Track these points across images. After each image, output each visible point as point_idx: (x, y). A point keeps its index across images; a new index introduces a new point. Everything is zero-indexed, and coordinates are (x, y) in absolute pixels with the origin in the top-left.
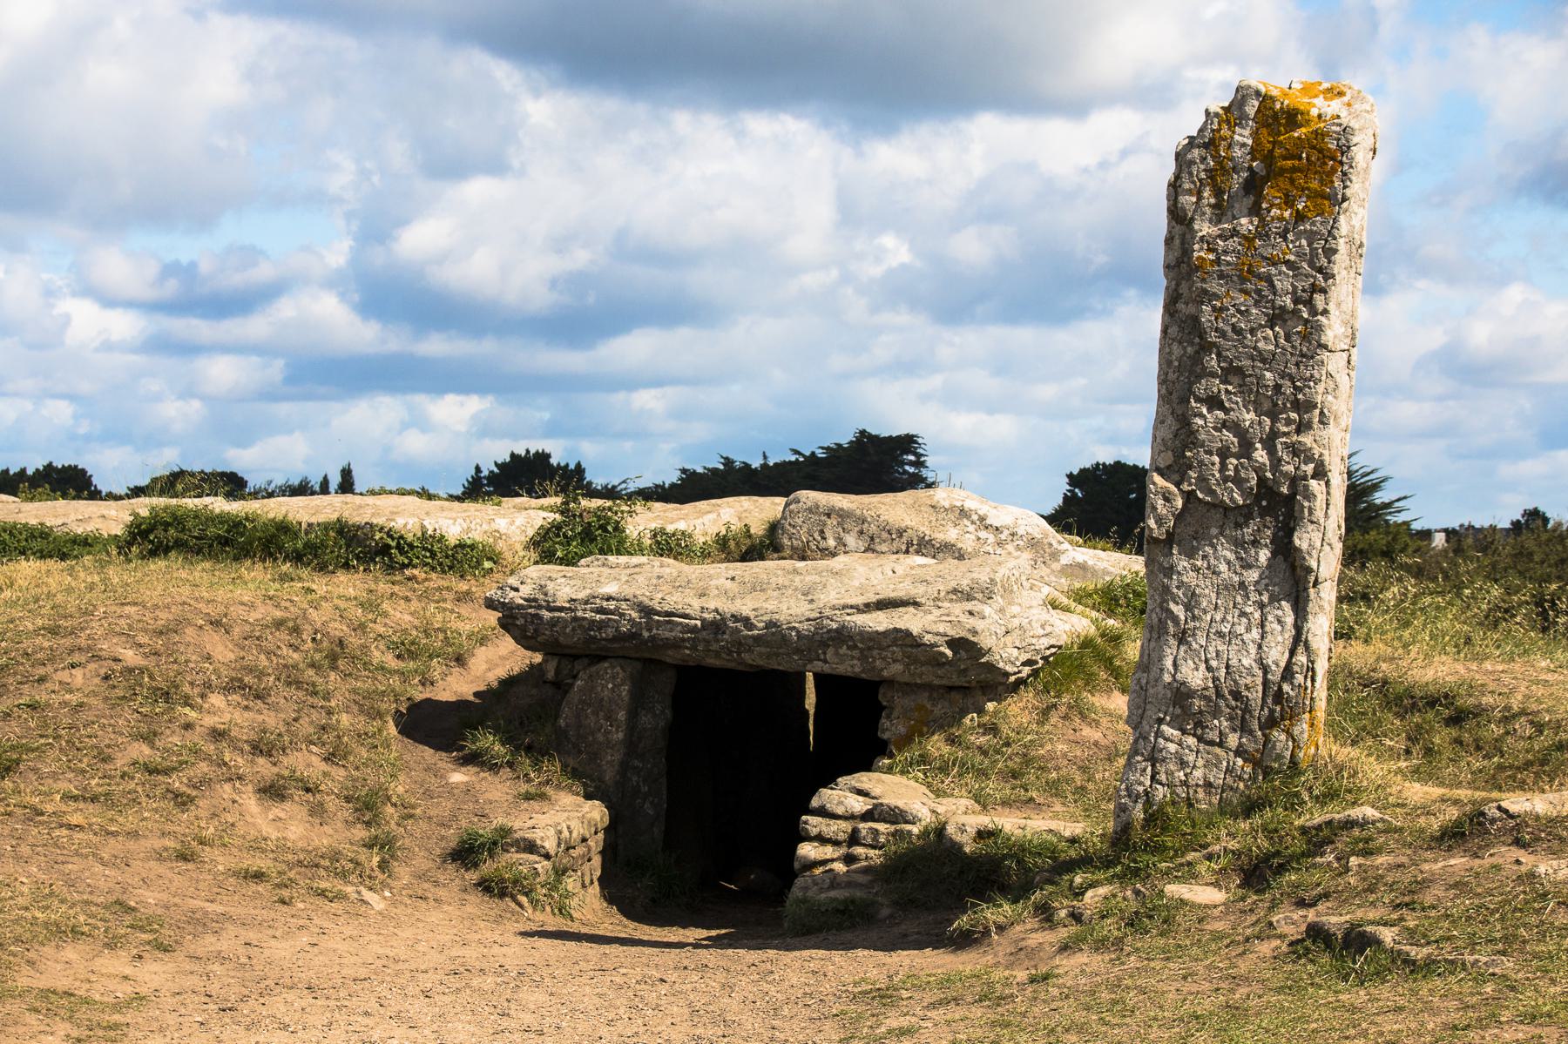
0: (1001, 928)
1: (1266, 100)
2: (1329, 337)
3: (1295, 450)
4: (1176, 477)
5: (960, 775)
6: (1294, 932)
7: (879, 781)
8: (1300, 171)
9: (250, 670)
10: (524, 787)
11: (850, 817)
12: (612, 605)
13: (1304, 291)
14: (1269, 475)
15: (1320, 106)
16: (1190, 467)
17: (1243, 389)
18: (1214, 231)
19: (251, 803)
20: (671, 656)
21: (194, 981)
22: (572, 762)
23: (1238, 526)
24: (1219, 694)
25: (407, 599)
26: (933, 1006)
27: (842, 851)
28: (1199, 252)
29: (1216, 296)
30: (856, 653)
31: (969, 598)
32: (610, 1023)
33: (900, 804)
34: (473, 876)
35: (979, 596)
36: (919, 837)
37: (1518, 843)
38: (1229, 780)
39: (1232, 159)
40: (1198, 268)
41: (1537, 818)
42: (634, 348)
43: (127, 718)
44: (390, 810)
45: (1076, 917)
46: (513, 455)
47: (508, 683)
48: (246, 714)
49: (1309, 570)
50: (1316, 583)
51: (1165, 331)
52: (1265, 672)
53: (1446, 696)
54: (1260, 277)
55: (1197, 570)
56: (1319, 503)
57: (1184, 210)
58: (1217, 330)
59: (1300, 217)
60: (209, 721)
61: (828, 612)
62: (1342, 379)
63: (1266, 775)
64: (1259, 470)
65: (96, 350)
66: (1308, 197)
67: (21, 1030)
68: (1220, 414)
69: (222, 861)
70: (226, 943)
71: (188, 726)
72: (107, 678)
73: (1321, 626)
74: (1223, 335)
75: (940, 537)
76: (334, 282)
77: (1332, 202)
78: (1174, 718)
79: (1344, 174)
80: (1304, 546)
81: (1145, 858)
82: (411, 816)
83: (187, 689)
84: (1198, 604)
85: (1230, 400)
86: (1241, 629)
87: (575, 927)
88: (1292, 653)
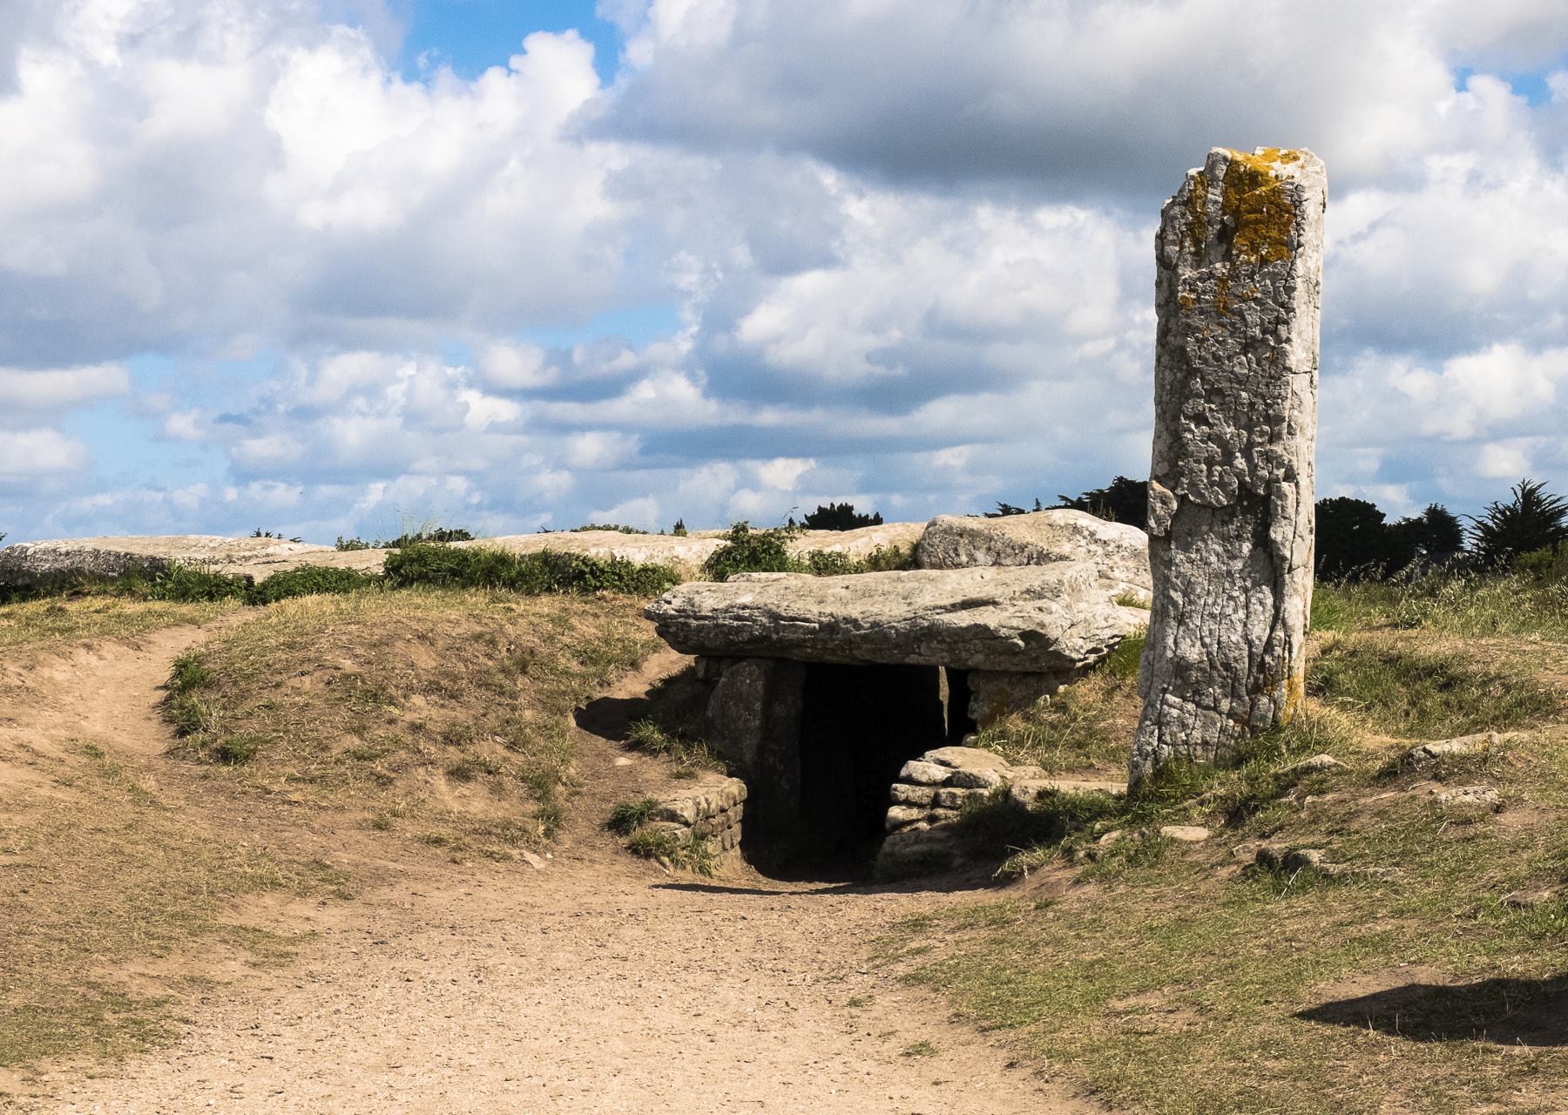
0: (1032, 869)
1: (1232, 164)
2: (1292, 361)
3: (1269, 458)
4: (1172, 484)
5: (1033, 747)
6: (1248, 858)
7: (962, 753)
9: (446, 675)
10: (675, 768)
11: (932, 784)
12: (747, 613)
15: (1278, 169)
16: (1183, 475)
17: (1223, 407)
19: (441, 783)
20: (796, 655)
21: (363, 923)
22: (717, 746)
23: (1224, 523)
24: (1213, 667)
25: (596, 616)
26: (953, 931)
27: (926, 812)
28: (1183, 293)
29: (1198, 330)
30: (944, 646)
31: (1040, 596)
32: (686, 950)
33: (975, 771)
34: (624, 841)
35: (1049, 595)
36: (989, 799)
37: (1437, 778)
38: (1223, 739)
39: (1206, 214)
41: (1453, 756)
42: (941, 413)
43: (343, 715)
44: (560, 788)
45: (1091, 856)
46: (820, 509)
47: (669, 682)
48: (443, 711)
49: (1284, 559)
50: (1290, 570)
51: (1158, 360)
52: (1250, 647)
53: (1442, 666)
54: (1233, 312)
55: (1192, 562)
56: (1291, 498)
59: (1264, 261)
60: (409, 717)
61: (921, 612)
62: (1306, 396)
63: (1252, 733)
64: (1240, 475)
65: (486, 432)
67: (211, 956)
69: (410, 829)
70: (399, 893)
71: (391, 721)
72: (329, 683)
73: (1298, 606)
74: (1205, 361)
75: (1056, 550)
76: (687, 368)
77: (1289, 247)
80: (1279, 539)
81: (1148, 806)
82: (578, 793)
83: (392, 691)
84: (1194, 590)
86: (1229, 611)
87: (715, 883)
88: (1272, 629)
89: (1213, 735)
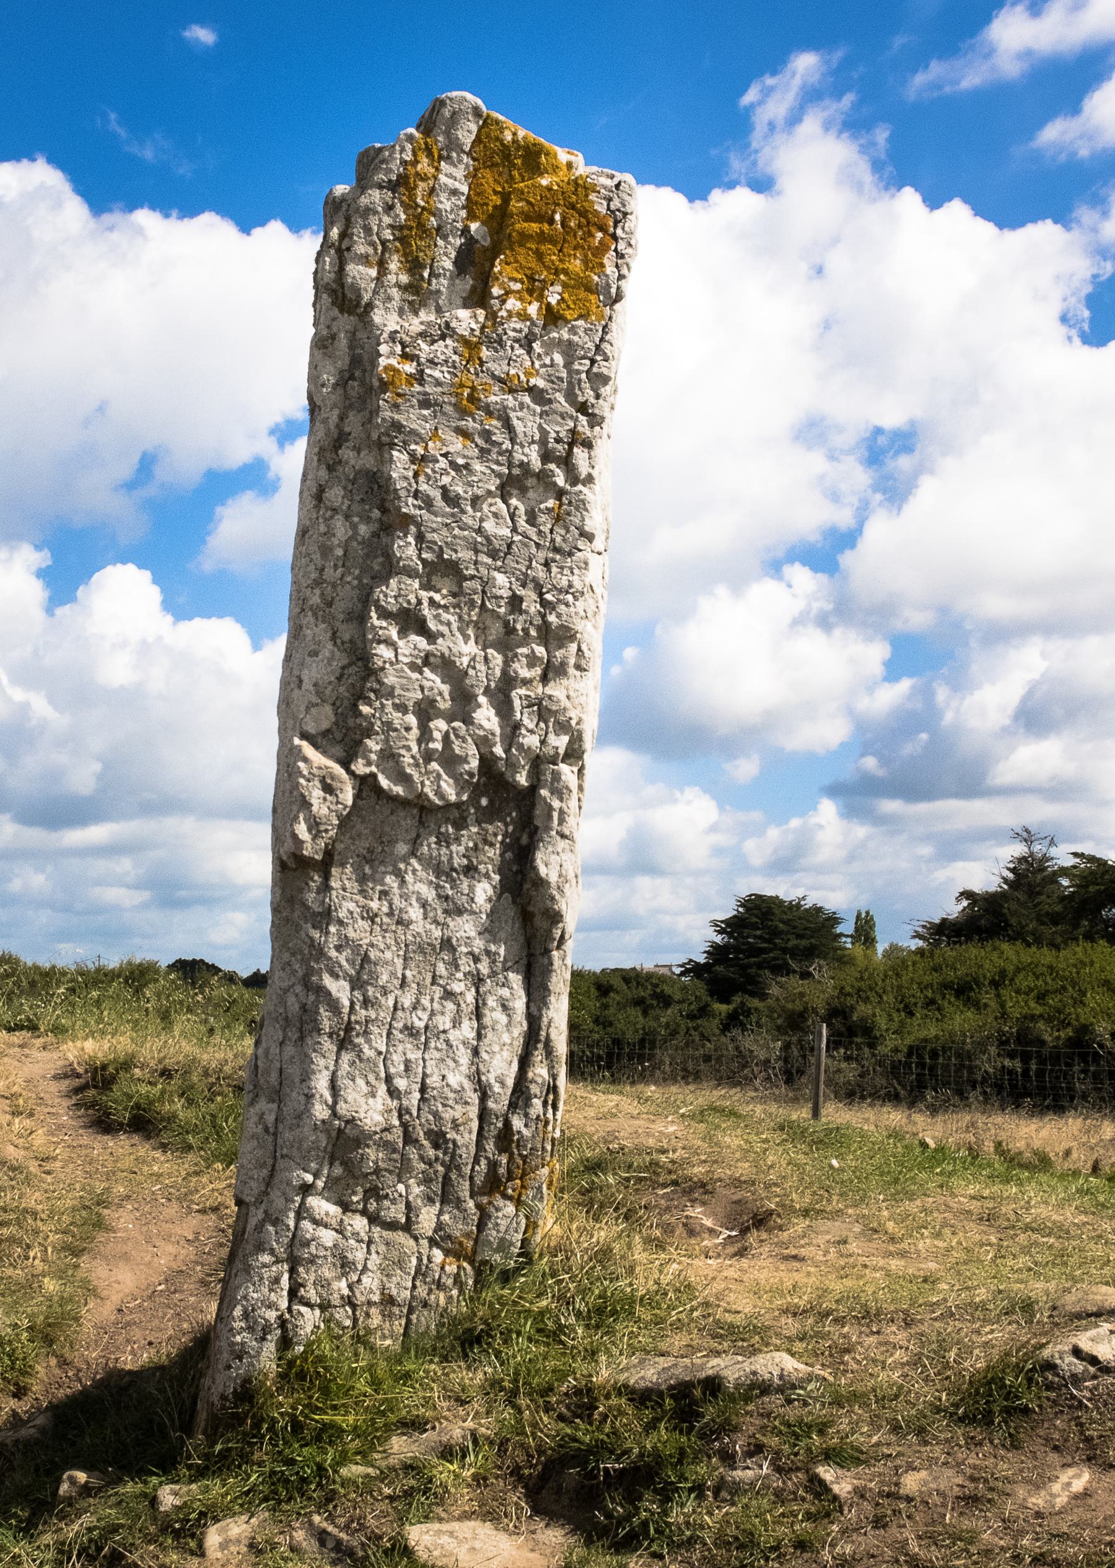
3: (543, 711)
8: (552, 241)
13: (558, 440)
14: (499, 750)
16: (369, 732)
18: (415, 325)
23: (444, 840)
24: (409, 1138)
28: (388, 358)
40: (384, 386)
55: (372, 917)
57: (357, 291)
58: (416, 494)
59: (552, 317)
64: (483, 742)
66: (565, 286)
68: (422, 642)
78: (332, 1183)
79: (620, 255)
80: (553, 878)
85: (437, 617)
86: (443, 1022)
88: (525, 1062)
89: (401, 1287)
